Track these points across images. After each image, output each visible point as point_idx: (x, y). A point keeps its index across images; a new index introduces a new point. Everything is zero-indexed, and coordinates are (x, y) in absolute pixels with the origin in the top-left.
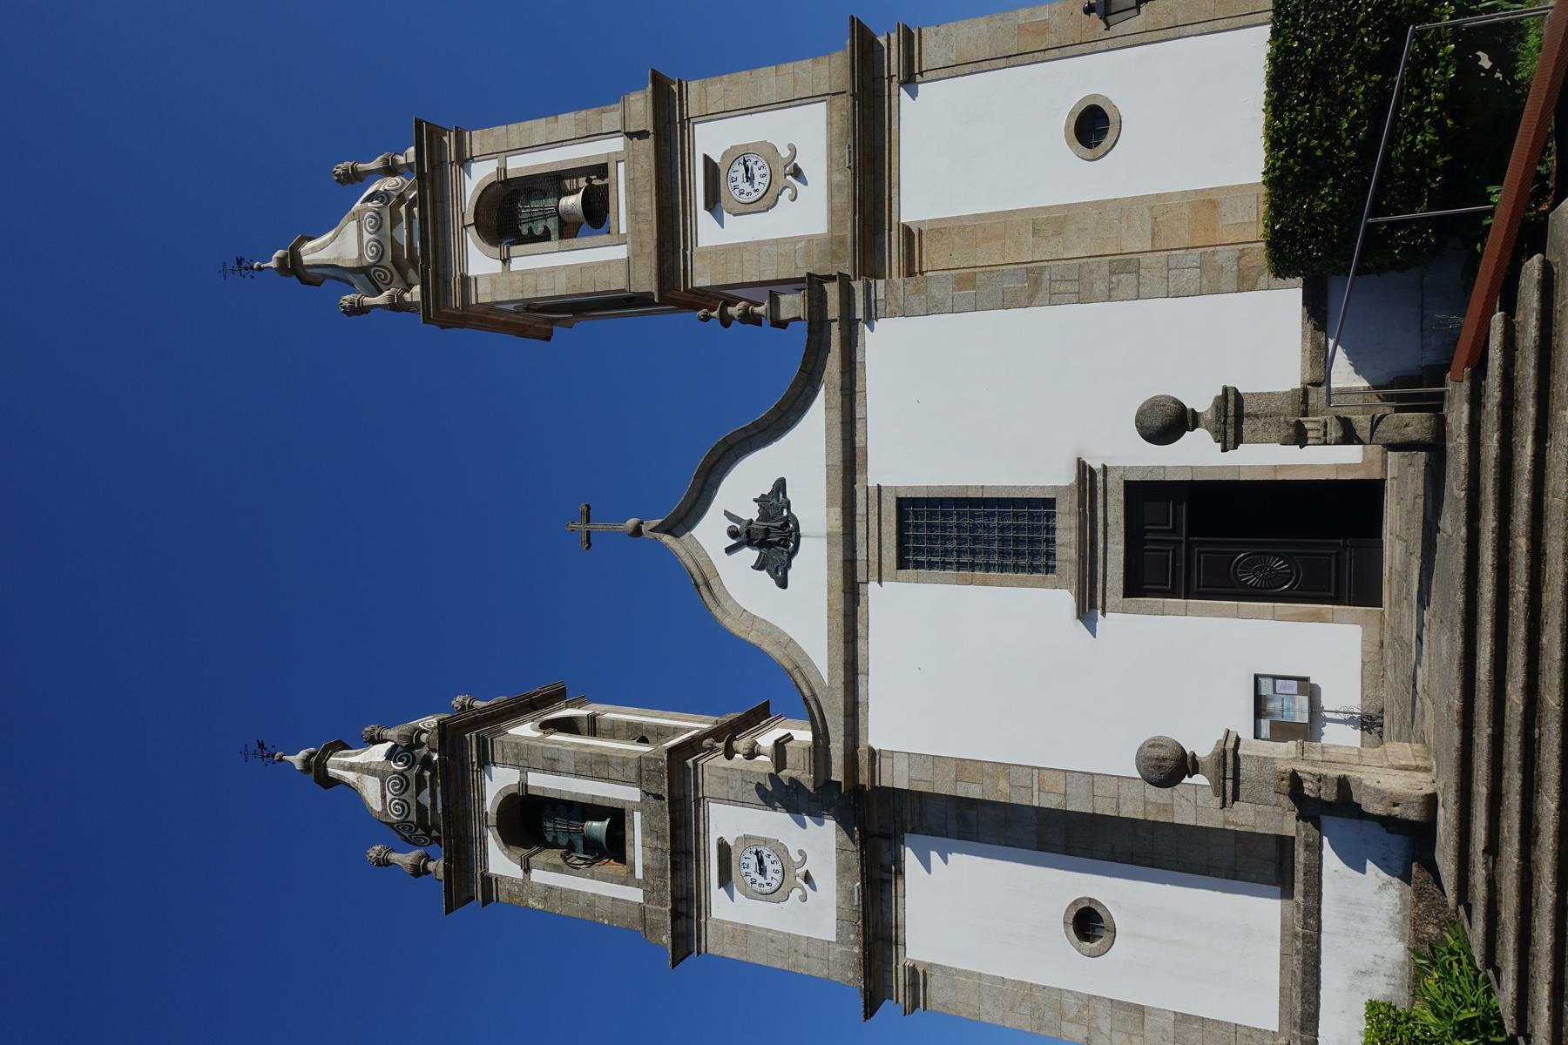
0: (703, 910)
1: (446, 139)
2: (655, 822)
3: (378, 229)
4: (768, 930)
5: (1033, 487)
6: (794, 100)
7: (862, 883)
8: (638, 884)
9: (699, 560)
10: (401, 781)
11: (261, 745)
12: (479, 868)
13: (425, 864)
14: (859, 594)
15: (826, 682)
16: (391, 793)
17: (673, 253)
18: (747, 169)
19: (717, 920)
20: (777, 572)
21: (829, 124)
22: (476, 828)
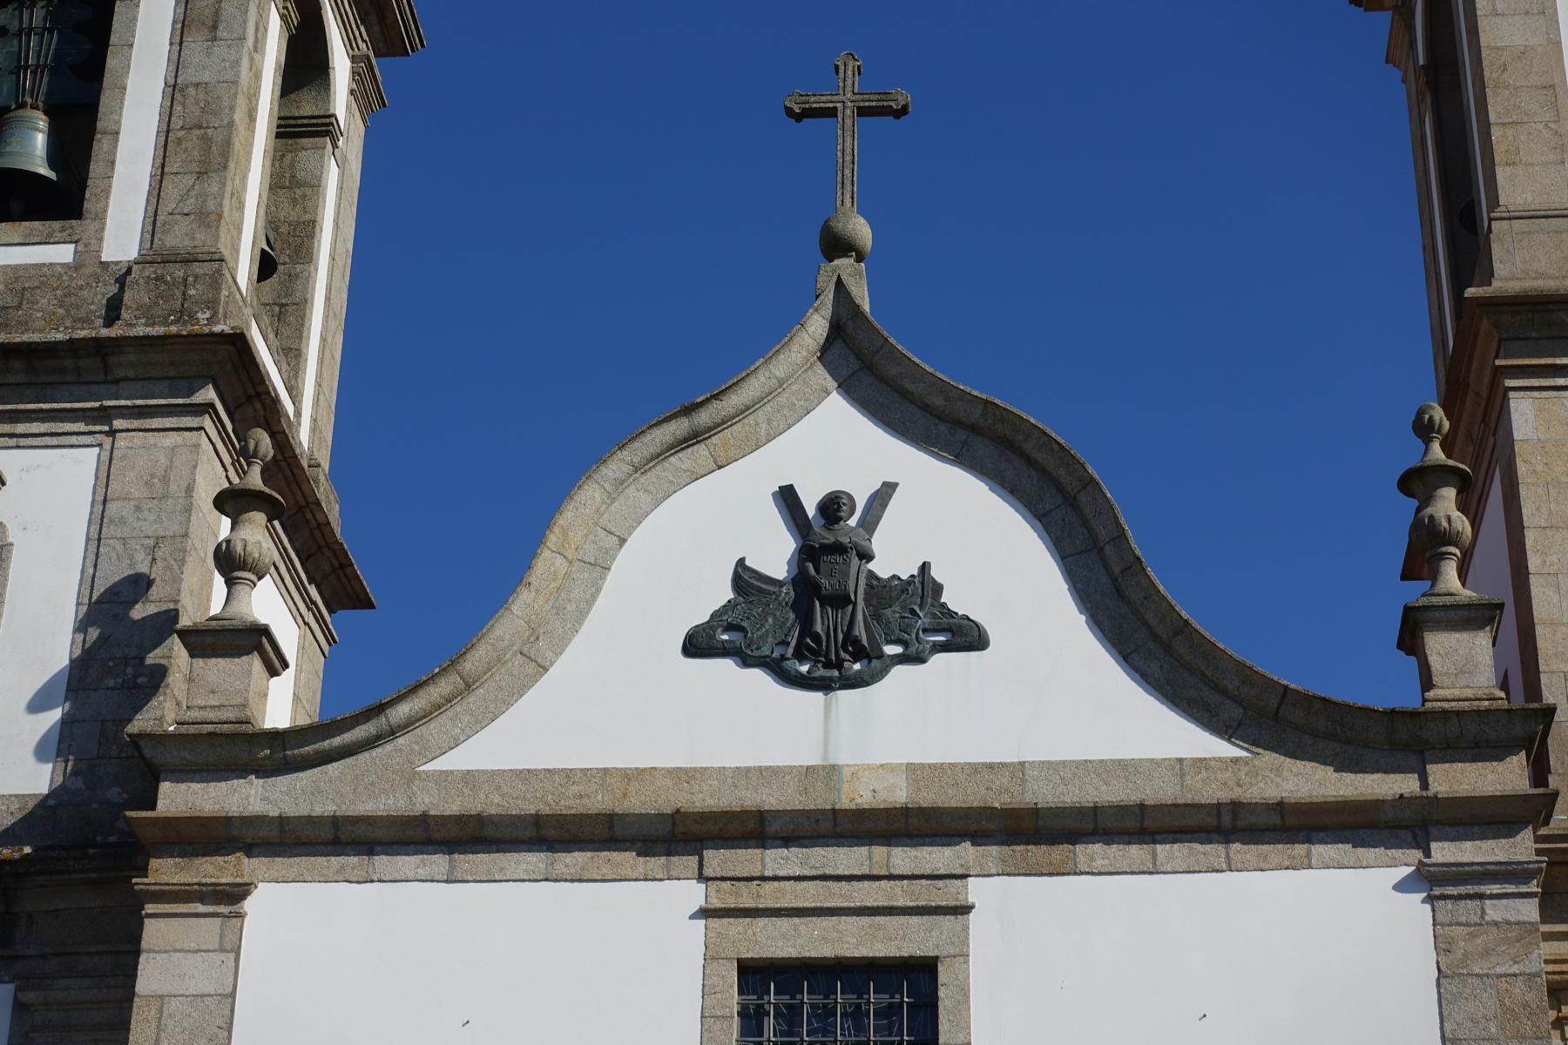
2: (46, 301)
9: (761, 416)
20: (730, 628)
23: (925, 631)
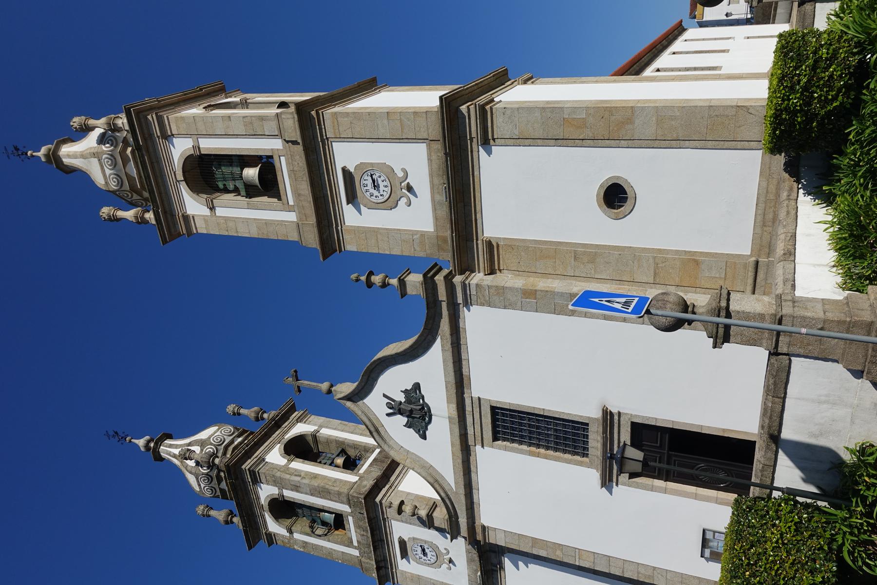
0: (394, 566)
1: (149, 117)
2: (361, 523)
3: (115, 166)
4: (431, 579)
5: (575, 415)
6: (403, 139)
7: (481, 573)
8: (355, 548)
9: (371, 417)
10: (208, 478)
11: (17, 149)
12: (263, 529)
13: (231, 519)
14: (470, 450)
15: (454, 489)
16: (108, 168)
17: (329, 226)
18: (374, 181)
19: (402, 571)
20: (419, 431)
21: (430, 160)
22: (257, 511)
23: (416, 394)
